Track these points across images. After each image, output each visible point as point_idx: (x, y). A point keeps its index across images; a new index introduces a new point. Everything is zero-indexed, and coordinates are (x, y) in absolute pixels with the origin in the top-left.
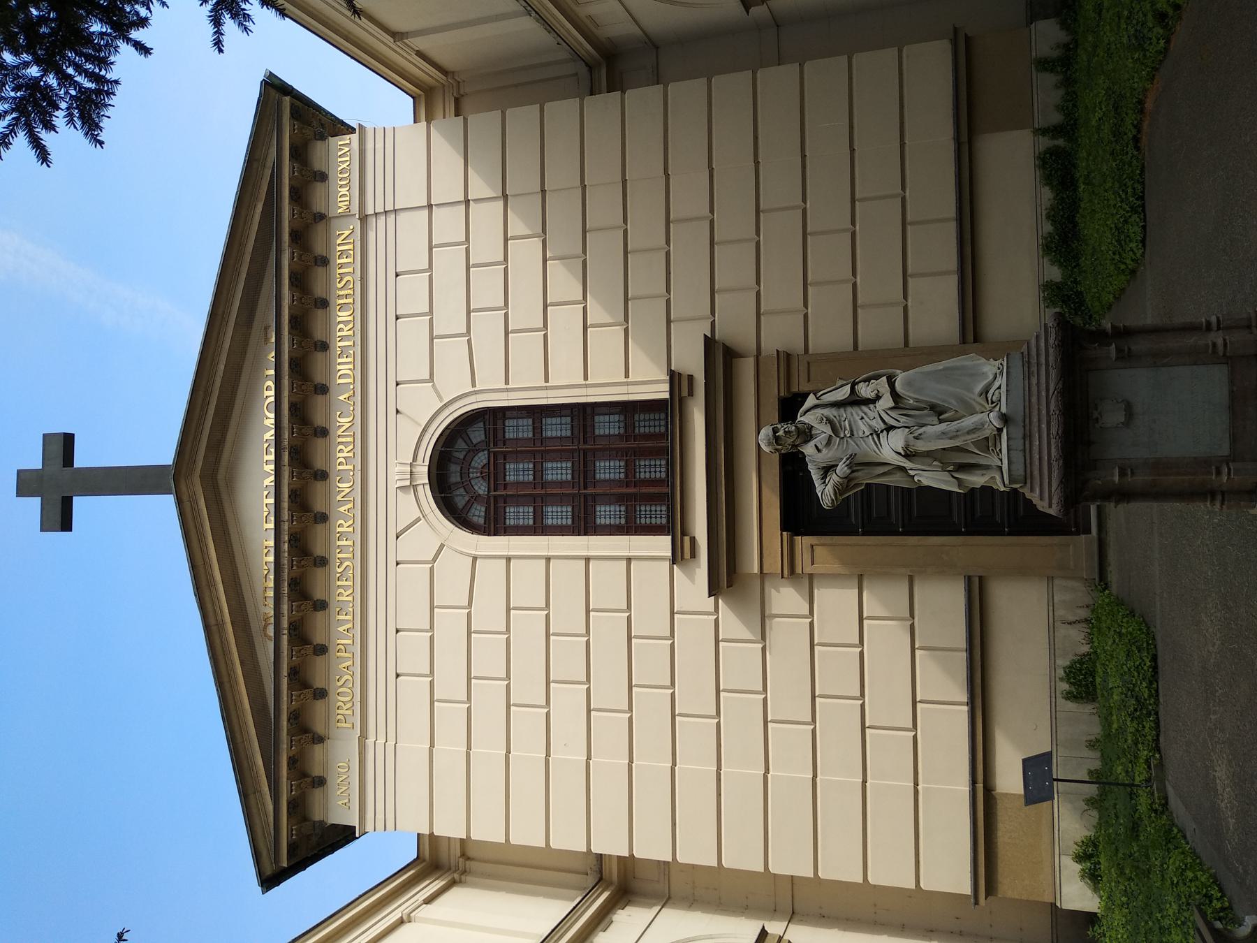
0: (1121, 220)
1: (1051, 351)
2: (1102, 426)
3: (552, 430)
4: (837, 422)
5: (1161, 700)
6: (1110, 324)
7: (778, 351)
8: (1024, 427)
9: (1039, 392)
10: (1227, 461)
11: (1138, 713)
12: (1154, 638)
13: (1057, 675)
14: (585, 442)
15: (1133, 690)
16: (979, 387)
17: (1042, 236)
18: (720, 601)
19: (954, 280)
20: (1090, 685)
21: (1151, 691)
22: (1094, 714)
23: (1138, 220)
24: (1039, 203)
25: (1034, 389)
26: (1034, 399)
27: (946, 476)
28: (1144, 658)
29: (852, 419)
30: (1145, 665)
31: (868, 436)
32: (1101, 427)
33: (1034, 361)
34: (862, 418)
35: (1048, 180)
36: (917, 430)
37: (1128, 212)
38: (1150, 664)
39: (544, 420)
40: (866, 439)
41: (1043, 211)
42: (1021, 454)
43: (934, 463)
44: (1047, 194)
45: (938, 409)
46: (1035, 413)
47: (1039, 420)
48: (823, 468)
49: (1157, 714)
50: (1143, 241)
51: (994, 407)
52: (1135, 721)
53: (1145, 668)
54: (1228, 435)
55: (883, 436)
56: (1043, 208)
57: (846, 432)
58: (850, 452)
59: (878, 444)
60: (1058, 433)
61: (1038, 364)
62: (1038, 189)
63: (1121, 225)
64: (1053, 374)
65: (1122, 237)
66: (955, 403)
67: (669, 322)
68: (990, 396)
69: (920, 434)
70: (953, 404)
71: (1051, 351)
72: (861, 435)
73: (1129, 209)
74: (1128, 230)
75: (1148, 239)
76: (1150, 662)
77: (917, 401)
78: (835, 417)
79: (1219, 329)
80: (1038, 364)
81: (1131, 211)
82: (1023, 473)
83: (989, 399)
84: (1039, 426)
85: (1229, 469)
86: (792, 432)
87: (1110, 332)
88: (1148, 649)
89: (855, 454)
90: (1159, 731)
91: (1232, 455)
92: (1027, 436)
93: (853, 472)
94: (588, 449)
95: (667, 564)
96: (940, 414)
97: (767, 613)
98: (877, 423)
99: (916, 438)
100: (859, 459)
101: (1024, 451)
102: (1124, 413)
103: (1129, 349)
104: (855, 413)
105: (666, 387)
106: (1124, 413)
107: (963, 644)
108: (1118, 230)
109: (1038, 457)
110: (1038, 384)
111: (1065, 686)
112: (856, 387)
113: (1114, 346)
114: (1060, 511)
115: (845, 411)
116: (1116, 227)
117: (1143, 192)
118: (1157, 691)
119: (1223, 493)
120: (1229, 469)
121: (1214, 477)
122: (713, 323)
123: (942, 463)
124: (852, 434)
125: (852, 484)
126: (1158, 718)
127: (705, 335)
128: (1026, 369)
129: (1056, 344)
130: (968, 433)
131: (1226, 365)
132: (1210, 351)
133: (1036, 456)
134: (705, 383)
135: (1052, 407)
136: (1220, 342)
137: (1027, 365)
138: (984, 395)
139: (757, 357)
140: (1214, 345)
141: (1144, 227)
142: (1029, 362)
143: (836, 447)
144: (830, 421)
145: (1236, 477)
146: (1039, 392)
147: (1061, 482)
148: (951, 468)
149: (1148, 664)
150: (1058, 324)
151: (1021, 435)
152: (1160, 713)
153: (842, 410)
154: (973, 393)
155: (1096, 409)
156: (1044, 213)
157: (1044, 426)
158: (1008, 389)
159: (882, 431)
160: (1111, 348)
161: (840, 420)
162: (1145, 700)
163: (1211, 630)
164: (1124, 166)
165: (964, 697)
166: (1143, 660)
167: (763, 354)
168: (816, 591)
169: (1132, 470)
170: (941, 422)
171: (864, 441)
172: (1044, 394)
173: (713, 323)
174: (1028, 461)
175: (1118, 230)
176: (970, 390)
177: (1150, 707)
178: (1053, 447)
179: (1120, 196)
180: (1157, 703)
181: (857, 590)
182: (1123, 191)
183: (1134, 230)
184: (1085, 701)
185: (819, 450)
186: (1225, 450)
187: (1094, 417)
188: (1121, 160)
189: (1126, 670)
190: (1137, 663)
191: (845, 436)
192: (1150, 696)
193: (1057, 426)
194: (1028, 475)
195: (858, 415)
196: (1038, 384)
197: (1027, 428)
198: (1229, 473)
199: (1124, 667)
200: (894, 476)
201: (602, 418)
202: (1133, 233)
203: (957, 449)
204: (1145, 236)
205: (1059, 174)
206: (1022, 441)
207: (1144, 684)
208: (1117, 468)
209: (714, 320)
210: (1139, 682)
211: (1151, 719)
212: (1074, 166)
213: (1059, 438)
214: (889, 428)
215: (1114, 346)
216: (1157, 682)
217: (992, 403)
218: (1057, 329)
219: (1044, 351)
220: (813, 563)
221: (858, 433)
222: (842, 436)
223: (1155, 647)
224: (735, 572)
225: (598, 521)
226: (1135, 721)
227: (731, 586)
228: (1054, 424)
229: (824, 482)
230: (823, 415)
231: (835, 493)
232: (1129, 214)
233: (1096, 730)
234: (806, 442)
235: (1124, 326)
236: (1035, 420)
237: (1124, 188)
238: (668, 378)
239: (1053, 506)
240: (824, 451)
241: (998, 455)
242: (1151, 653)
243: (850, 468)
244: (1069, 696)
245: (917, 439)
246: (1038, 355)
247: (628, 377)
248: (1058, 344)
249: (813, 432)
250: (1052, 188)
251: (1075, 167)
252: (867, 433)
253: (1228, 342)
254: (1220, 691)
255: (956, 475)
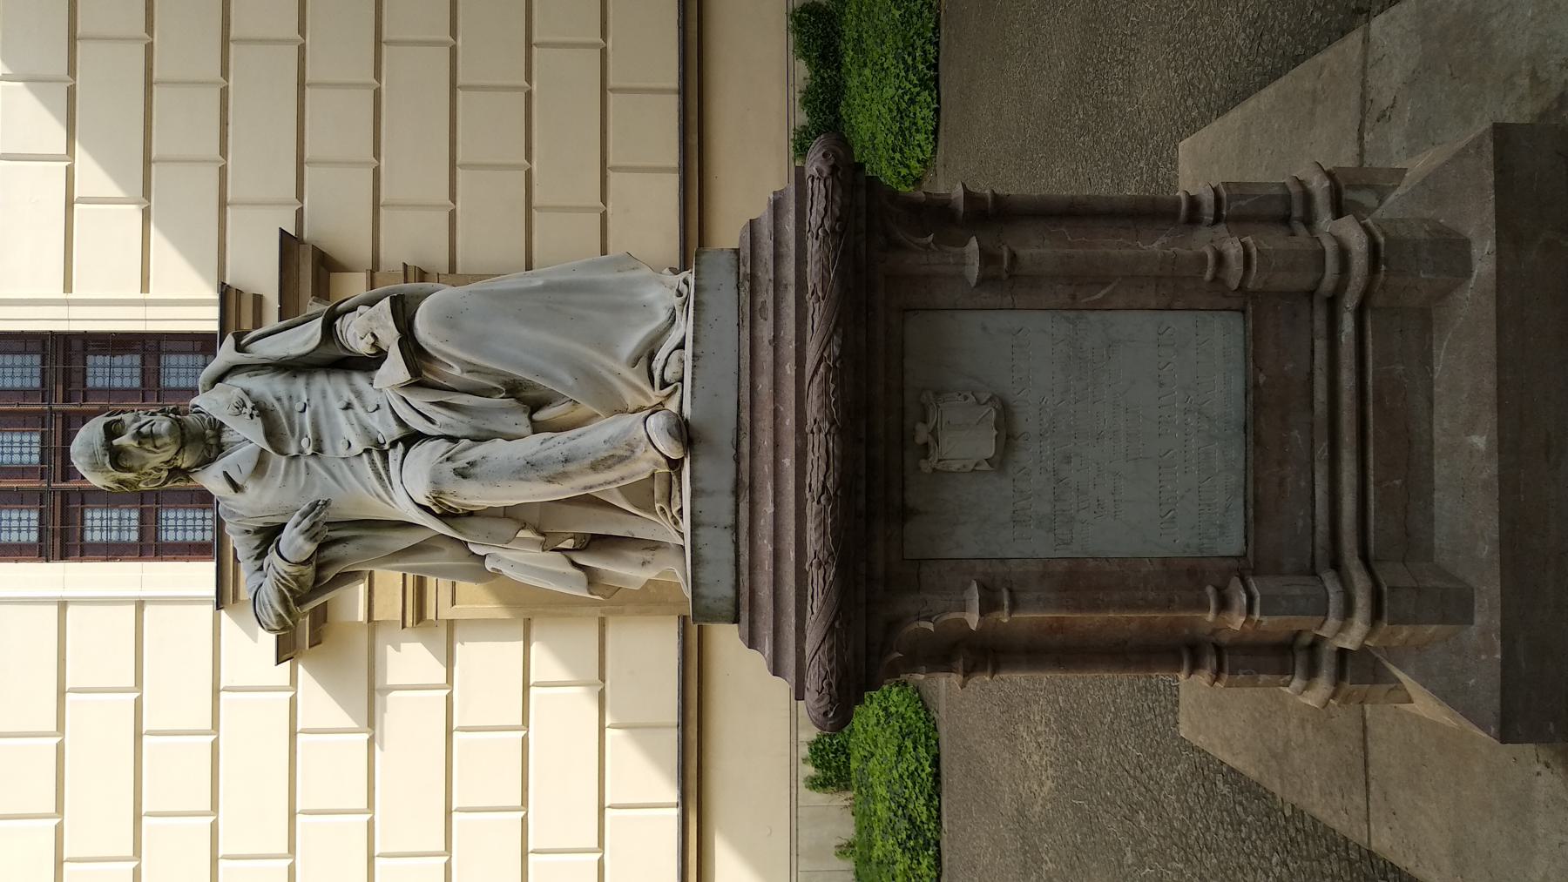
0: (906, 98)
1: (813, 246)
2: (939, 467)
3: (122, 377)
4: (281, 413)
5: (945, 825)
6: (959, 188)
7: (405, 266)
8: (737, 460)
9: (777, 364)
10: (1246, 567)
11: (912, 843)
12: (935, 729)
13: (799, 755)
14: (67, 400)
15: (904, 808)
16: (632, 342)
17: (795, 129)
18: (300, 667)
19: (674, 180)
20: (842, 767)
21: (930, 812)
22: (846, 807)
23: (929, 99)
24: (791, 82)
25: (766, 355)
26: (764, 384)
27: (557, 563)
28: (922, 760)
29: (321, 410)
30: (923, 770)
31: (360, 455)
32: (934, 470)
33: (766, 275)
34: (348, 407)
35: (803, 50)
36: (465, 450)
37: (915, 86)
38: (930, 770)
39: (162, 358)
40: (354, 462)
41: (796, 93)
42: (726, 538)
43: (522, 534)
44: (802, 70)
45: (530, 394)
46: (766, 423)
47: (776, 446)
48: (258, 531)
49: (937, 844)
50: (935, 132)
51: (669, 396)
52: (908, 855)
53: (923, 775)
54: (1241, 501)
55: (395, 455)
56: (797, 90)
57: (304, 442)
58: (316, 495)
59: (383, 478)
60: (824, 486)
61: (778, 284)
62: (791, 60)
63: (904, 105)
64: (817, 312)
65: (907, 124)
66: (570, 382)
67: (223, 204)
68: (657, 365)
69: (472, 464)
70: (561, 380)
71: (813, 246)
72: (342, 450)
73: (916, 82)
74: (915, 114)
75: (942, 129)
76: (930, 767)
77: (473, 369)
78: (279, 399)
79: (1218, 219)
80: (778, 284)
81: (920, 86)
82: (730, 593)
83: (657, 374)
84: (776, 462)
85: (1251, 598)
86: (159, 436)
87: (961, 208)
88: (926, 745)
89: (326, 503)
90: (941, 871)
91: (1250, 557)
92: (745, 488)
93: (321, 547)
94: (71, 411)
95: (209, 609)
96: (535, 406)
97: (378, 685)
98: (383, 421)
99: (462, 474)
100: (332, 515)
101: (736, 528)
102: (995, 432)
103: (1014, 257)
104: (331, 390)
105: (214, 312)
106: (995, 432)
107: (672, 717)
108: (901, 113)
109: (770, 548)
110: (776, 340)
111: (810, 770)
112: (338, 322)
113: (974, 244)
114: (825, 714)
115: (308, 384)
116: (898, 108)
117: (937, 58)
118: (939, 810)
119: (1219, 649)
120: (1251, 598)
121: (1210, 616)
122: (300, 214)
123: (543, 534)
124: (318, 451)
125: (330, 574)
126: (939, 851)
127: (282, 231)
128: (745, 296)
129: (827, 225)
130: (595, 467)
131: (1238, 316)
132: (1208, 276)
133: (766, 547)
134: (280, 308)
135: (813, 409)
136: (1233, 249)
137: (747, 284)
138: (643, 362)
139: (372, 272)
140: (1220, 258)
141: (937, 111)
142: (753, 278)
143: (280, 478)
144: (262, 411)
145: (1265, 619)
146: (777, 364)
147: (831, 630)
148: (569, 544)
149: (928, 770)
150: (834, 169)
151: (727, 482)
152: (941, 843)
153: (300, 382)
154: (615, 357)
155: (925, 422)
156: (798, 97)
157: (788, 462)
158: (698, 352)
159: (394, 444)
160: (967, 249)
161: (292, 408)
162: (922, 822)
163: (1036, 758)
164: (912, 17)
165: (673, 796)
166: (921, 764)
167: (383, 268)
168: (458, 646)
169: (1010, 591)
170: (537, 428)
171: (351, 468)
172: (790, 369)
173: (300, 214)
174: (745, 559)
175: (901, 113)
176: (606, 346)
177: (929, 835)
178: (811, 525)
179: (905, 62)
180: (939, 831)
181: (522, 642)
182: (909, 54)
183: (923, 113)
184: (835, 789)
185: (236, 487)
186: (1233, 543)
187: (920, 440)
188: (907, 8)
189: (897, 776)
190: (912, 768)
191: (301, 452)
192: (930, 817)
193: (824, 466)
194: (745, 600)
195: (340, 398)
196: (776, 340)
197: (745, 464)
198: (1250, 609)
199: (894, 772)
200: (436, 555)
201: (173, 359)
202: (922, 119)
203: (589, 501)
204: (937, 125)
205: (819, 43)
206: (730, 500)
207: (922, 801)
208: (975, 586)
209: (302, 208)
210: (914, 797)
211: (930, 852)
212: (839, 34)
213: (829, 500)
214: (411, 439)
215: (974, 244)
216: (939, 796)
217: (664, 385)
218: (829, 182)
219: (792, 245)
220: (453, 603)
221: (334, 448)
222: (293, 451)
223: (937, 744)
224: (325, 621)
225: (88, 536)
226: (908, 855)
227: (319, 643)
228: (815, 457)
229: (261, 569)
230: (247, 393)
231: (284, 601)
232: (918, 89)
233: (847, 830)
234: (206, 462)
235: (995, 196)
236: (766, 441)
237: (910, 49)
238: (216, 297)
239: (807, 694)
240: (252, 490)
241: (676, 523)
242: (932, 753)
243: (312, 538)
244: (815, 784)
245: (464, 477)
246: (778, 257)
247: (148, 292)
248: (833, 230)
249: (225, 438)
250: (809, 63)
251: (839, 37)
252: (358, 448)
253: (1254, 251)
254: (1050, 864)
255: (581, 559)
